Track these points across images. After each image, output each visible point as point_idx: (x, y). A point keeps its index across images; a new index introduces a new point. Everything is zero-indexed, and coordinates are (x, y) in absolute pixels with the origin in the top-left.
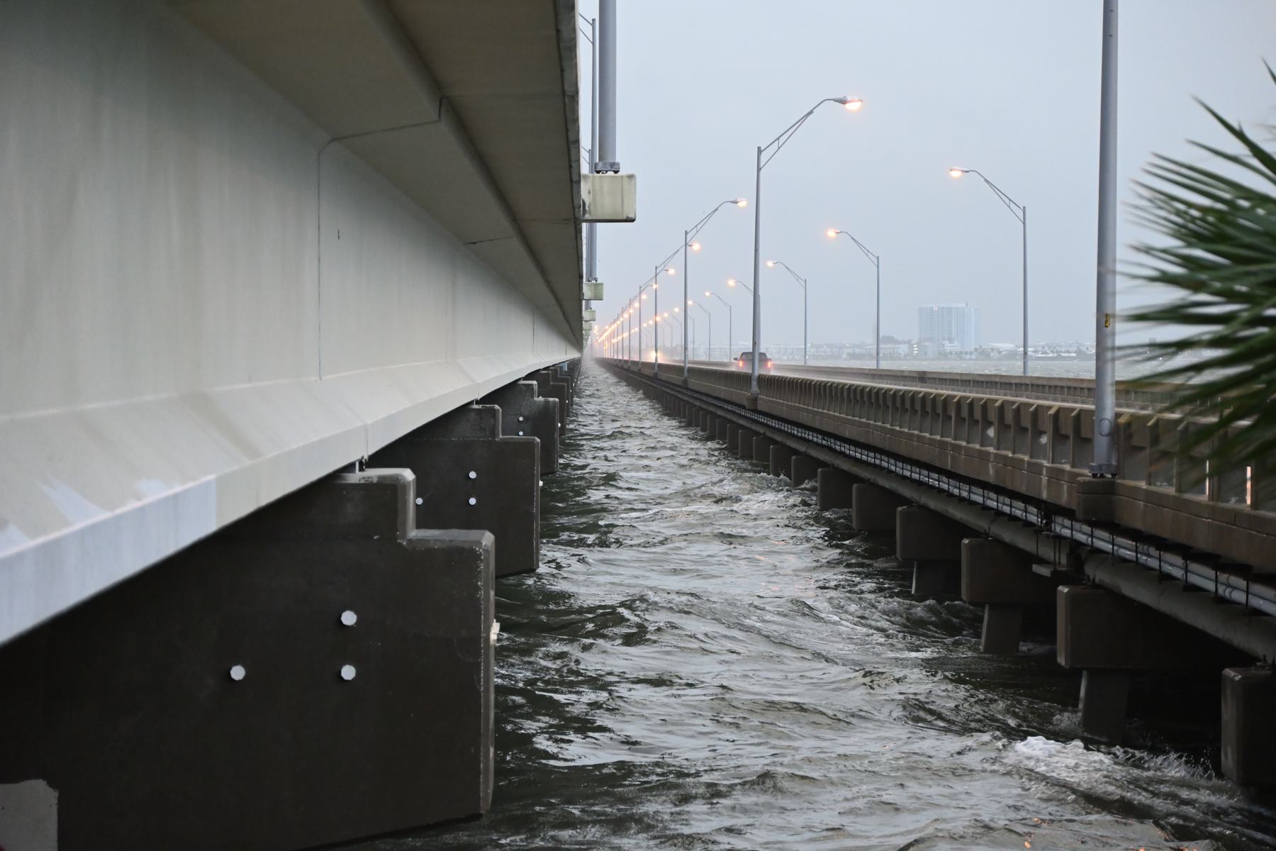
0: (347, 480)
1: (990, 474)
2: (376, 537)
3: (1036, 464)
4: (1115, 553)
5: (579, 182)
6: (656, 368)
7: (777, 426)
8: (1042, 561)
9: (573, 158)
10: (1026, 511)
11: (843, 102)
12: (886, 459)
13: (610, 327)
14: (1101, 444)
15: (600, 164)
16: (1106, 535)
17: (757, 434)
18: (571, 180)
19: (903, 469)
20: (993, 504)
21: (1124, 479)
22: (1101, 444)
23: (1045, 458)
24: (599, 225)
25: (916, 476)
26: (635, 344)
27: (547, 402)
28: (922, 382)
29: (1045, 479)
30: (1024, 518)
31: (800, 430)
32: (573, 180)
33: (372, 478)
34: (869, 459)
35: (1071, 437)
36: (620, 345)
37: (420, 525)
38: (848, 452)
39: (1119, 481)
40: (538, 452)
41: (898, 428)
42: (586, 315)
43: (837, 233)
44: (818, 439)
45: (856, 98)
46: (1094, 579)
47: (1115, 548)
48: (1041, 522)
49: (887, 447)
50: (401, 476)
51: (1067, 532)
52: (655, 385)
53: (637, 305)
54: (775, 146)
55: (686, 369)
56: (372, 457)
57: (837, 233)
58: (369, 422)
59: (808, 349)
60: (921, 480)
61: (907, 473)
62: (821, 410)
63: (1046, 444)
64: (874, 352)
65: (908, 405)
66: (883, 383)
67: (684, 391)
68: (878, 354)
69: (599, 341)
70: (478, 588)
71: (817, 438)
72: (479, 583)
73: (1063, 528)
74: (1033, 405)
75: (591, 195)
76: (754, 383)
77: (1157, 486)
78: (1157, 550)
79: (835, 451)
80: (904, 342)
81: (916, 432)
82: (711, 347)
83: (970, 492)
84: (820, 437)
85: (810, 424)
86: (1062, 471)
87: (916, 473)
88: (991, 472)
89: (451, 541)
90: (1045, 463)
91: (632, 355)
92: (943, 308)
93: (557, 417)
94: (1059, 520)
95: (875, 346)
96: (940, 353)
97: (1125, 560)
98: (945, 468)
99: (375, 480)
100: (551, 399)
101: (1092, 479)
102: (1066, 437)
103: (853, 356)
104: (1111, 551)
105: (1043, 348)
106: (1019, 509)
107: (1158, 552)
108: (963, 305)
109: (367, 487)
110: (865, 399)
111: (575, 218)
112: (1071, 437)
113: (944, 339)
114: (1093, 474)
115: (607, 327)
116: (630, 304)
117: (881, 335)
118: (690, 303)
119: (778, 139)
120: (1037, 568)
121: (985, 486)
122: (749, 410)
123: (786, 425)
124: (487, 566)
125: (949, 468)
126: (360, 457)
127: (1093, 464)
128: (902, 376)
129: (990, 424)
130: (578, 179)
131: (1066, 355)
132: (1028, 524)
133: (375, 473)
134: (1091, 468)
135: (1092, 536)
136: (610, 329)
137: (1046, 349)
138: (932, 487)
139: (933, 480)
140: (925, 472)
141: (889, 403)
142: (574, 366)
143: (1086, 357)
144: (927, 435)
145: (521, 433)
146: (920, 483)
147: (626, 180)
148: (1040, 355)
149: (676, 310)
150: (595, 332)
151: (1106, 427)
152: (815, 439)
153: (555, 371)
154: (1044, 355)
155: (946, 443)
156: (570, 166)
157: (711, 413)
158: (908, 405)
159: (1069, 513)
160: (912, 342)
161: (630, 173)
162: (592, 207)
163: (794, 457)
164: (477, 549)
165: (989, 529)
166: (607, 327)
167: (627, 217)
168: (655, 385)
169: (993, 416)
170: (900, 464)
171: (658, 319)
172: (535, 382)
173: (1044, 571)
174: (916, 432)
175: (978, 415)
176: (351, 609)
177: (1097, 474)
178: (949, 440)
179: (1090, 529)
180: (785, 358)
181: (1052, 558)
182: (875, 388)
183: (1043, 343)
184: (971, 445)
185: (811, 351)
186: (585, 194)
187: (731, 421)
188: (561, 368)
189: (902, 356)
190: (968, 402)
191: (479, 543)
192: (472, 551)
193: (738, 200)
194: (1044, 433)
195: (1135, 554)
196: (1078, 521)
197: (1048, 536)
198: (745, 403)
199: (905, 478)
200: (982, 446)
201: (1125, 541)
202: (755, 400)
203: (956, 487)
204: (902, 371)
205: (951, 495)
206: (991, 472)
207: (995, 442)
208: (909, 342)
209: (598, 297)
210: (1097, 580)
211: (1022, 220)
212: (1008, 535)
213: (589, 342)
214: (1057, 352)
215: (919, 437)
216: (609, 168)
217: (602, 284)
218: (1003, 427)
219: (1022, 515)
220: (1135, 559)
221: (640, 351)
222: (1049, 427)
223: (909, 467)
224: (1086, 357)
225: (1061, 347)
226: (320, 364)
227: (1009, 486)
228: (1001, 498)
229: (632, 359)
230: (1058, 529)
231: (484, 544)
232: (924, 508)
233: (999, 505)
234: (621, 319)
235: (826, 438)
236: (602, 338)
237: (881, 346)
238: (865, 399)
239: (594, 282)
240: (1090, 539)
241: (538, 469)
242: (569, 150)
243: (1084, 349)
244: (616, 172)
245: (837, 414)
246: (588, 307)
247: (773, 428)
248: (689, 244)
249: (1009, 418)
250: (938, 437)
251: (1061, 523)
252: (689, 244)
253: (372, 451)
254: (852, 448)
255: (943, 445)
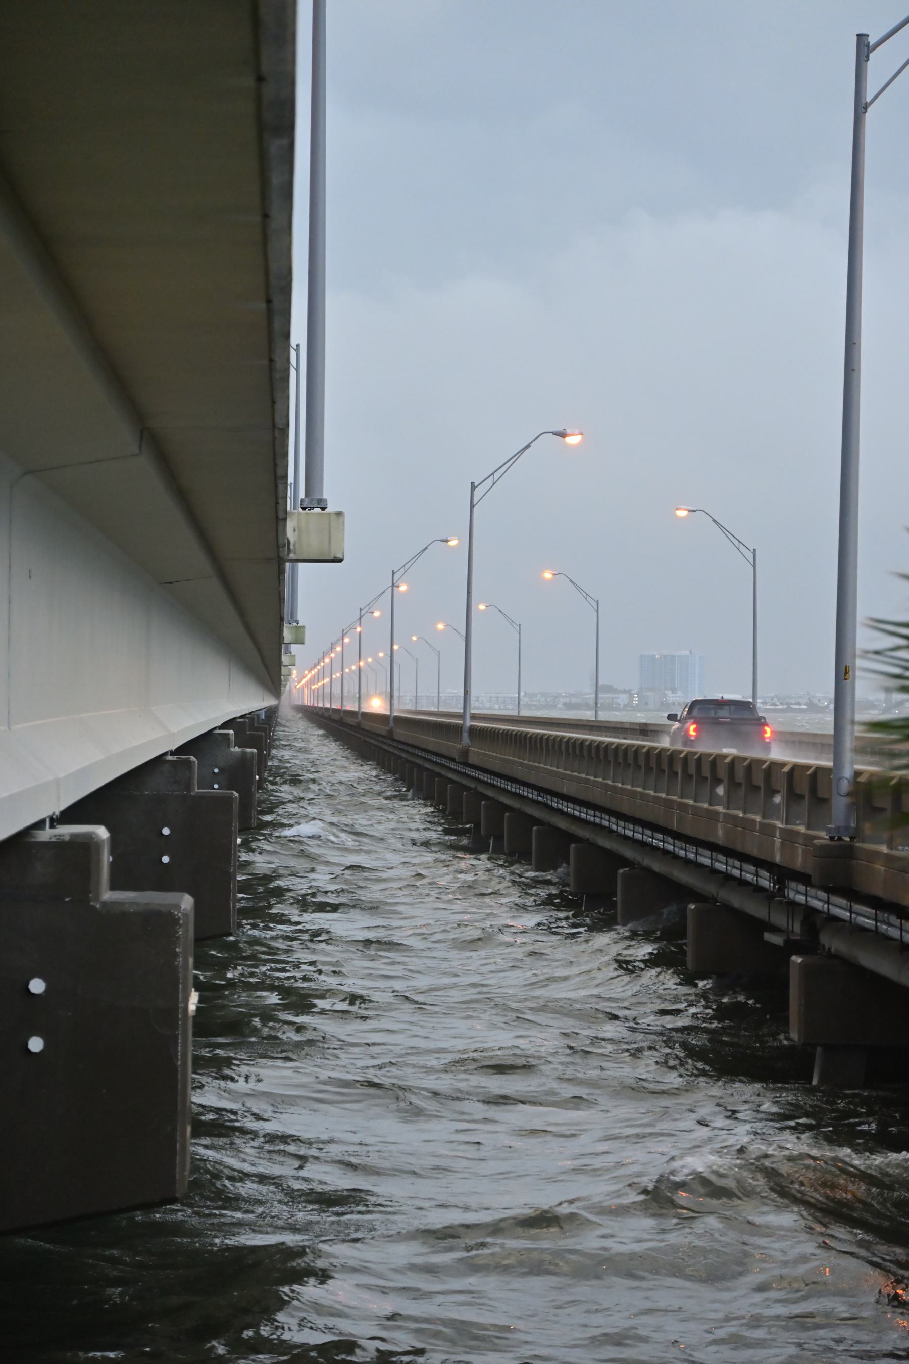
0: (36, 837)
1: (720, 835)
2: (67, 900)
3: (768, 825)
4: (853, 921)
5: (285, 520)
6: (360, 716)
7: (489, 781)
8: (775, 930)
9: (281, 494)
10: (757, 875)
11: (563, 435)
12: (607, 817)
13: (310, 671)
14: (840, 805)
15: (307, 500)
16: (843, 902)
17: (468, 789)
18: (277, 518)
19: (625, 828)
20: (722, 867)
21: (863, 842)
22: (840, 805)
23: (778, 818)
24: (301, 565)
25: (638, 836)
26: (337, 690)
27: (244, 753)
28: (644, 735)
29: (778, 841)
30: (755, 882)
31: (514, 785)
32: (279, 519)
33: (63, 835)
34: (588, 817)
35: (807, 798)
36: (321, 692)
37: (113, 887)
38: (565, 809)
39: (858, 844)
40: (236, 807)
41: (620, 785)
42: (285, 659)
43: (554, 575)
44: (533, 795)
45: (577, 431)
46: (829, 949)
47: (853, 916)
48: (774, 887)
49: (581, 796)
50: (94, 833)
51: (801, 899)
52: (358, 735)
53: (339, 649)
54: (489, 482)
55: (392, 719)
56: (63, 813)
57: (554, 575)
58: (62, 775)
59: (521, 698)
60: (729, 872)
61: (629, 833)
62: (537, 765)
63: (779, 804)
64: (592, 702)
65: (631, 760)
66: (601, 736)
67: (389, 742)
68: (596, 704)
69: (298, 687)
70: (176, 955)
71: (533, 794)
72: (177, 950)
73: (797, 893)
74: (766, 762)
75: (296, 532)
76: (465, 735)
77: (899, 850)
78: (898, 918)
79: (551, 808)
80: (624, 691)
81: (639, 789)
82: (418, 694)
83: (697, 854)
84: (536, 793)
85: (526, 779)
86: (798, 833)
87: (639, 832)
88: (720, 832)
89: (147, 904)
90: (779, 824)
91: (345, 703)
92: (665, 656)
93: (255, 769)
94: (793, 885)
95: (594, 696)
96: (662, 704)
97: (863, 929)
98: (769, 860)
99: (67, 838)
100: (249, 750)
101: (829, 843)
102: (801, 797)
103: (569, 706)
104: (848, 919)
105: (772, 699)
106: (749, 873)
107: (899, 921)
108: (687, 652)
109: (59, 846)
110: (585, 754)
111: (279, 557)
112: (807, 798)
113: (666, 689)
114: (830, 837)
115: (306, 672)
116: (332, 648)
117: (600, 683)
118: (396, 647)
119: (493, 474)
120: (768, 937)
121: (713, 847)
122: (459, 763)
123: (499, 780)
124: (187, 931)
125: (675, 828)
126: (50, 813)
127: (830, 826)
128: (622, 729)
129: (718, 782)
130: (284, 516)
131: (797, 707)
132: (759, 889)
133: (67, 830)
134: (829, 831)
135: (828, 903)
136: (310, 675)
137: (775, 700)
138: (656, 848)
139: (657, 840)
140: (649, 832)
141: (611, 758)
142: (272, 712)
143: (822, 710)
144: (652, 793)
145: (216, 786)
146: (643, 844)
147: (333, 517)
148: (768, 707)
149: (381, 655)
150: (294, 677)
151: (845, 787)
152: (530, 796)
153: (252, 719)
154: (773, 707)
155: (672, 801)
156: (277, 503)
157: (419, 766)
158: (631, 760)
159: (804, 878)
160: (633, 692)
161: (338, 509)
162: (297, 546)
163: (507, 814)
164: (176, 913)
165: (717, 895)
166: (306, 672)
167: (335, 557)
168: (358, 735)
169: (722, 773)
170: (622, 823)
171: (362, 664)
172: (231, 732)
173: (776, 939)
174: (639, 789)
175: (706, 772)
176: (40, 977)
177: (834, 837)
178: (675, 798)
179: (826, 895)
180: (497, 707)
181: (785, 925)
182: (595, 741)
183: (773, 694)
184: (699, 804)
185: (524, 700)
186: (290, 534)
187: (439, 775)
188: (258, 716)
189: (621, 706)
190: (696, 757)
191: (178, 907)
192: (170, 915)
193: (449, 538)
194: (778, 792)
195: (874, 923)
196: (812, 886)
197: (781, 903)
198: (456, 756)
199: (626, 838)
200: (710, 804)
201: (864, 908)
202: (465, 752)
203: (681, 848)
204: (622, 723)
205: (675, 857)
206: (720, 832)
207: (725, 799)
208: (628, 692)
209: (300, 641)
210: (833, 950)
211: (752, 563)
212: (738, 900)
213: (288, 687)
214: (787, 704)
215: (680, 804)
216: (315, 505)
217: (303, 627)
218: (733, 785)
219: (753, 879)
220: (874, 928)
221: (342, 699)
222: (782, 785)
223: (631, 827)
224: (822, 710)
225: (791, 698)
226: (9, 713)
227: (739, 848)
228: (730, 861)
229: (344, 708)
230: (792, 895)
231: (183, 907)
232: (648, 870)
233: (729, 868)
234: (322, 664)
235: (542, 794)
236: (301, 684)
237: (600, 695)
238: (585, 754)
239: (295, 624)
240: (826, 906)
241: (236, 825)
242: (276, 486)
243: (815, 701)
244: (323, 509)
245: (554, 769)
246: (288, 651)
247: (486, 783)
248: (396, 584)
249: (740, 776)
250: (663, 795)
251: (795, 889)
252: (396, 584)
253: (63, 806)
254: (571, 805)
255: (668, 804)
